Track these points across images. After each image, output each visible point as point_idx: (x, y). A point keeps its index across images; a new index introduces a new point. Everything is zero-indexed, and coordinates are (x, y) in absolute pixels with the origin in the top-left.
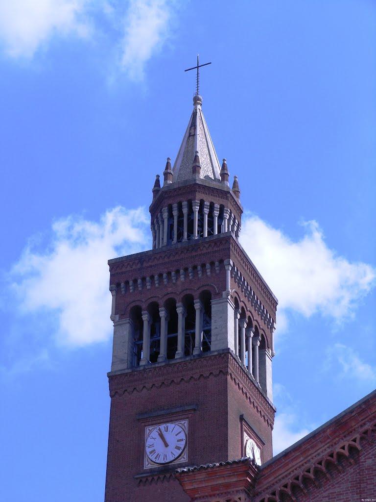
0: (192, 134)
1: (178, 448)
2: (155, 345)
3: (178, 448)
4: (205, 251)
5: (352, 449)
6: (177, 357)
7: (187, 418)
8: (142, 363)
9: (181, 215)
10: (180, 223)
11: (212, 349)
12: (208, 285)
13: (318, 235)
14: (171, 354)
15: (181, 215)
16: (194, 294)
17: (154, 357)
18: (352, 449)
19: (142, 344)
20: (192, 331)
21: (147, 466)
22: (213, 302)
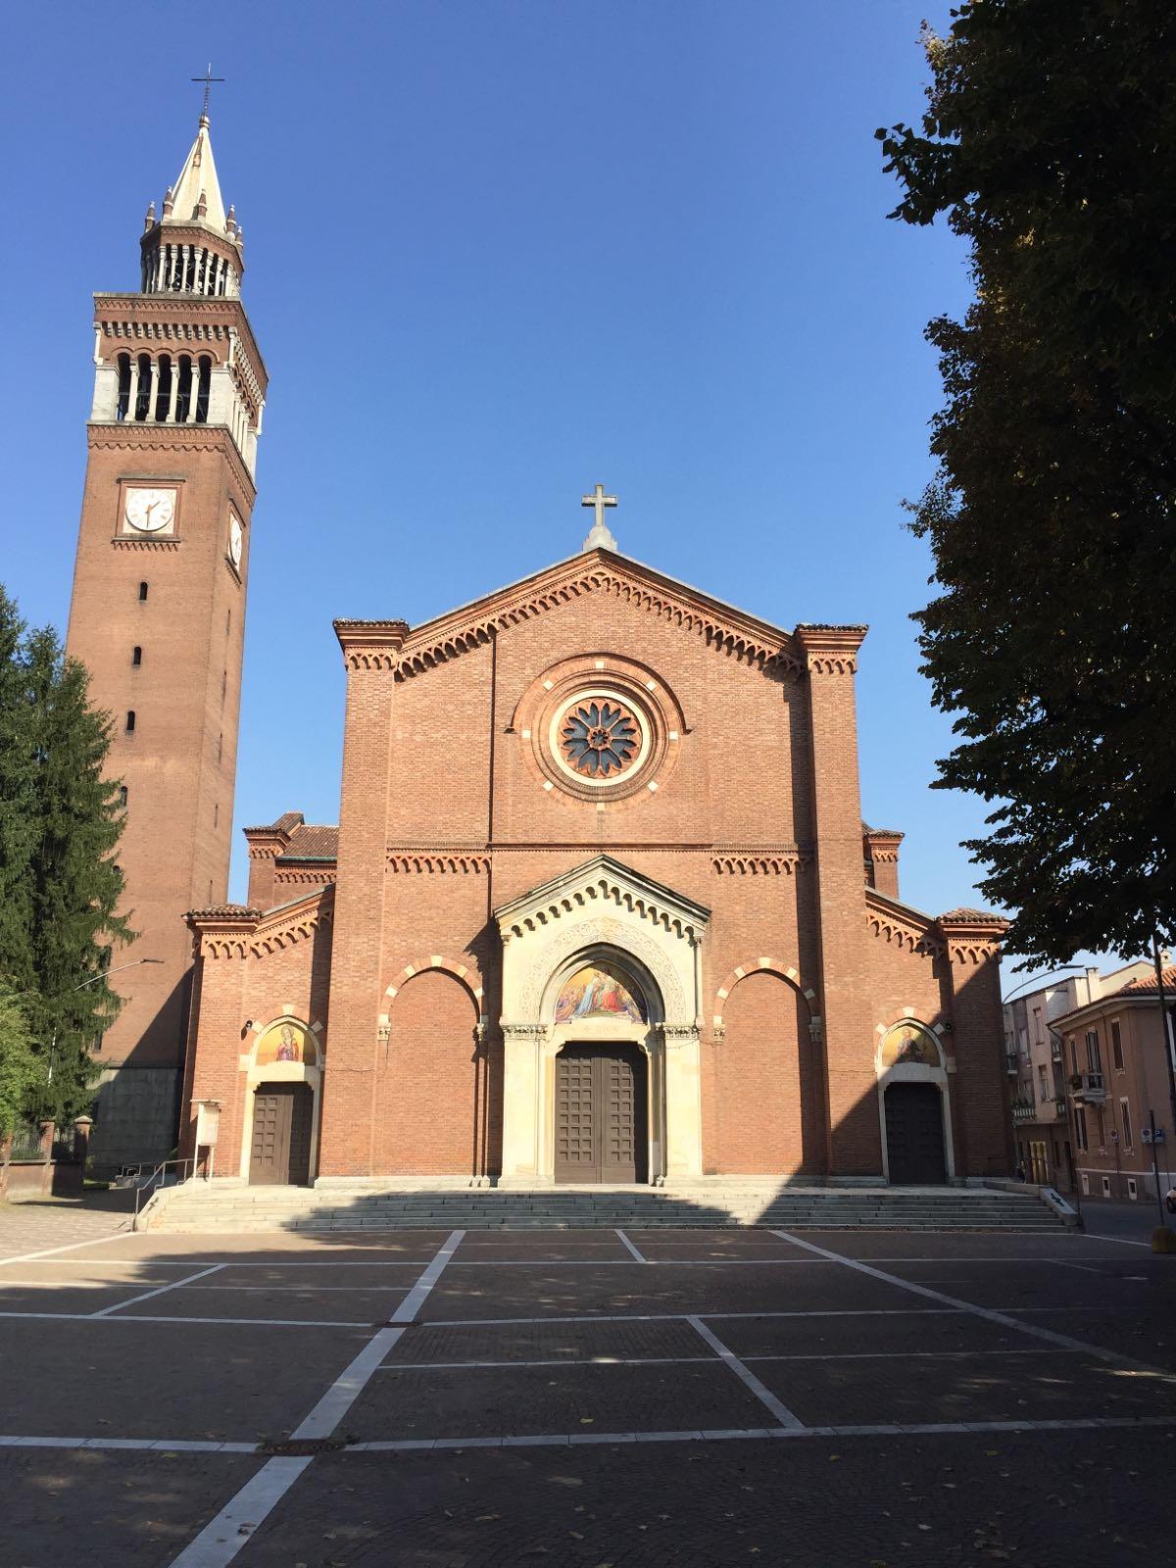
0: (197, 164)
1: (163, 518)
2: (143, 400)
3: (163, 518)
4: (208, 311)
5: (490, 627)
6: (167, 420)
7: (176, 488)
8: (127, 418)
9: (180, 260)
10: (179, 270)
11: (209, 420)
12: (213, 353)
13: (962, 323)
14: (161, 415)
15: (180, 260)
16: (151, 355)
17: (141, 414)
18: (490, 627)
19: (149, 397)
20: (167, 395)
21: (127, 530)
22: (213, 370)
